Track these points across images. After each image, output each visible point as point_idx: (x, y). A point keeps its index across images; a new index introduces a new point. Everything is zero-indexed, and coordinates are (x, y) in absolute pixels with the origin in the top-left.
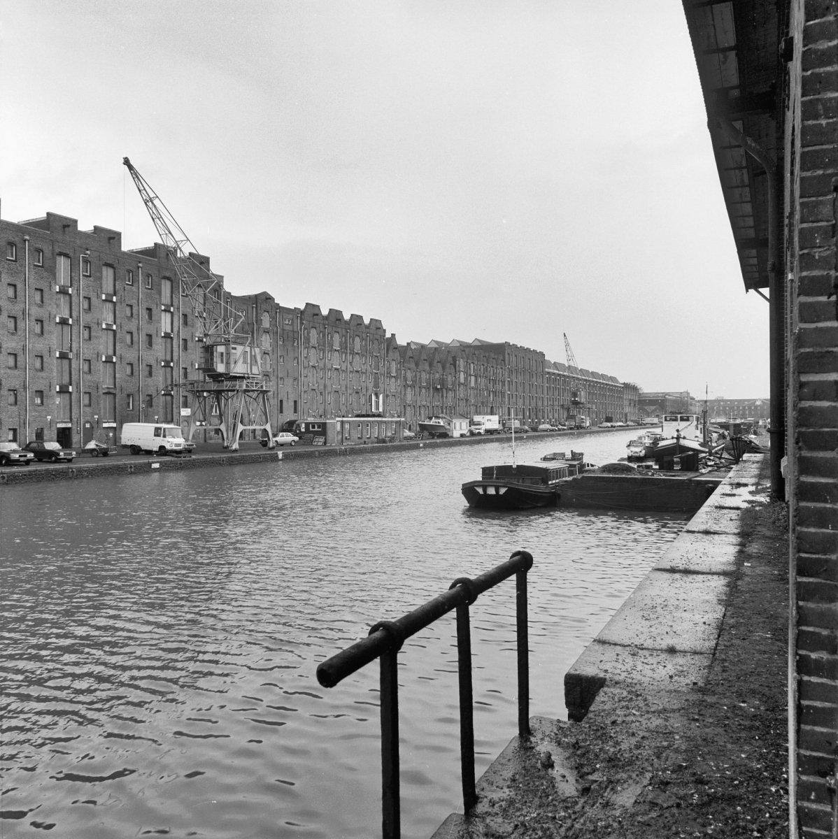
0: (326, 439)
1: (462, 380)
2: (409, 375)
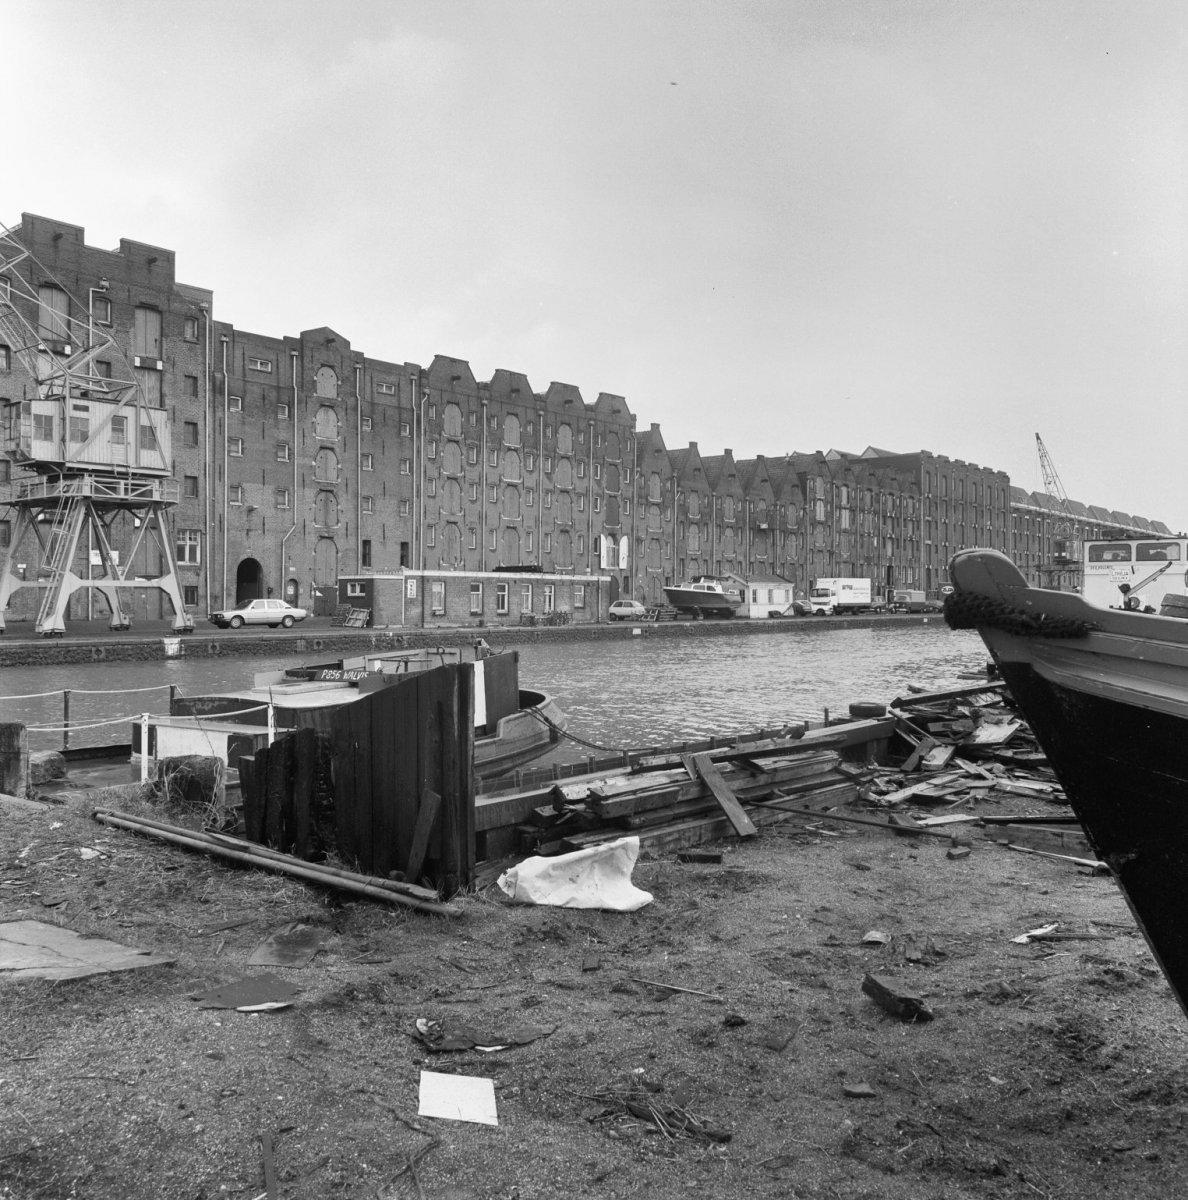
0: (371, 615)
1: (820, 515)
2: (693, 502)
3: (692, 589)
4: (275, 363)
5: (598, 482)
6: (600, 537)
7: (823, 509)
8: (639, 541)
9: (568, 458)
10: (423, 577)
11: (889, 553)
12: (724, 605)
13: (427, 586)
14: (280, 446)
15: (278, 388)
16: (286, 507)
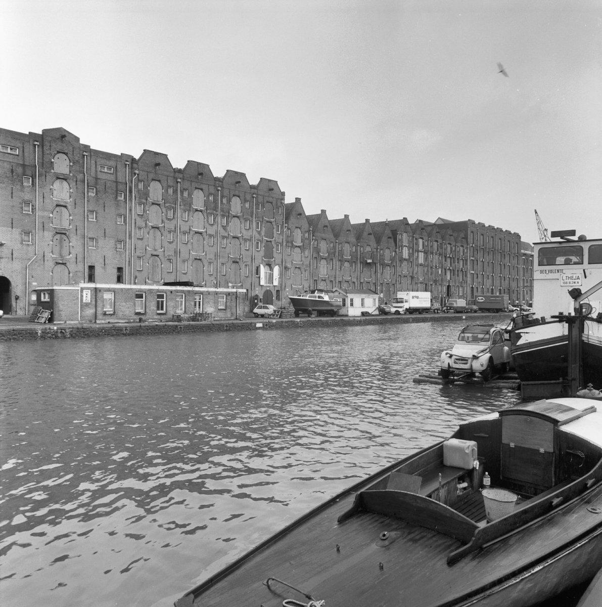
0: (52, 314)
2: (323, 246)
3: (307, 298)
4: (22, 150)
5: (259, 233)
6: (260, 266)
7: (407, 252)
8: (286, 268)
9: (238, 217)
10: (96, 288)
11: (449, 278)
12: (329, 308)
13: (99, 295)
14: (27, 203)
15: (24, 166)
16: (30, 243)
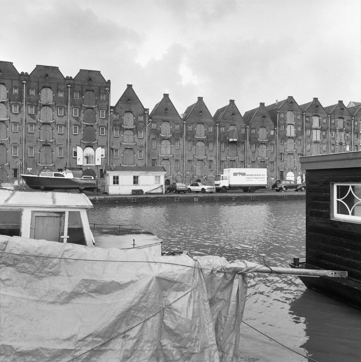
4: (302, 126)
